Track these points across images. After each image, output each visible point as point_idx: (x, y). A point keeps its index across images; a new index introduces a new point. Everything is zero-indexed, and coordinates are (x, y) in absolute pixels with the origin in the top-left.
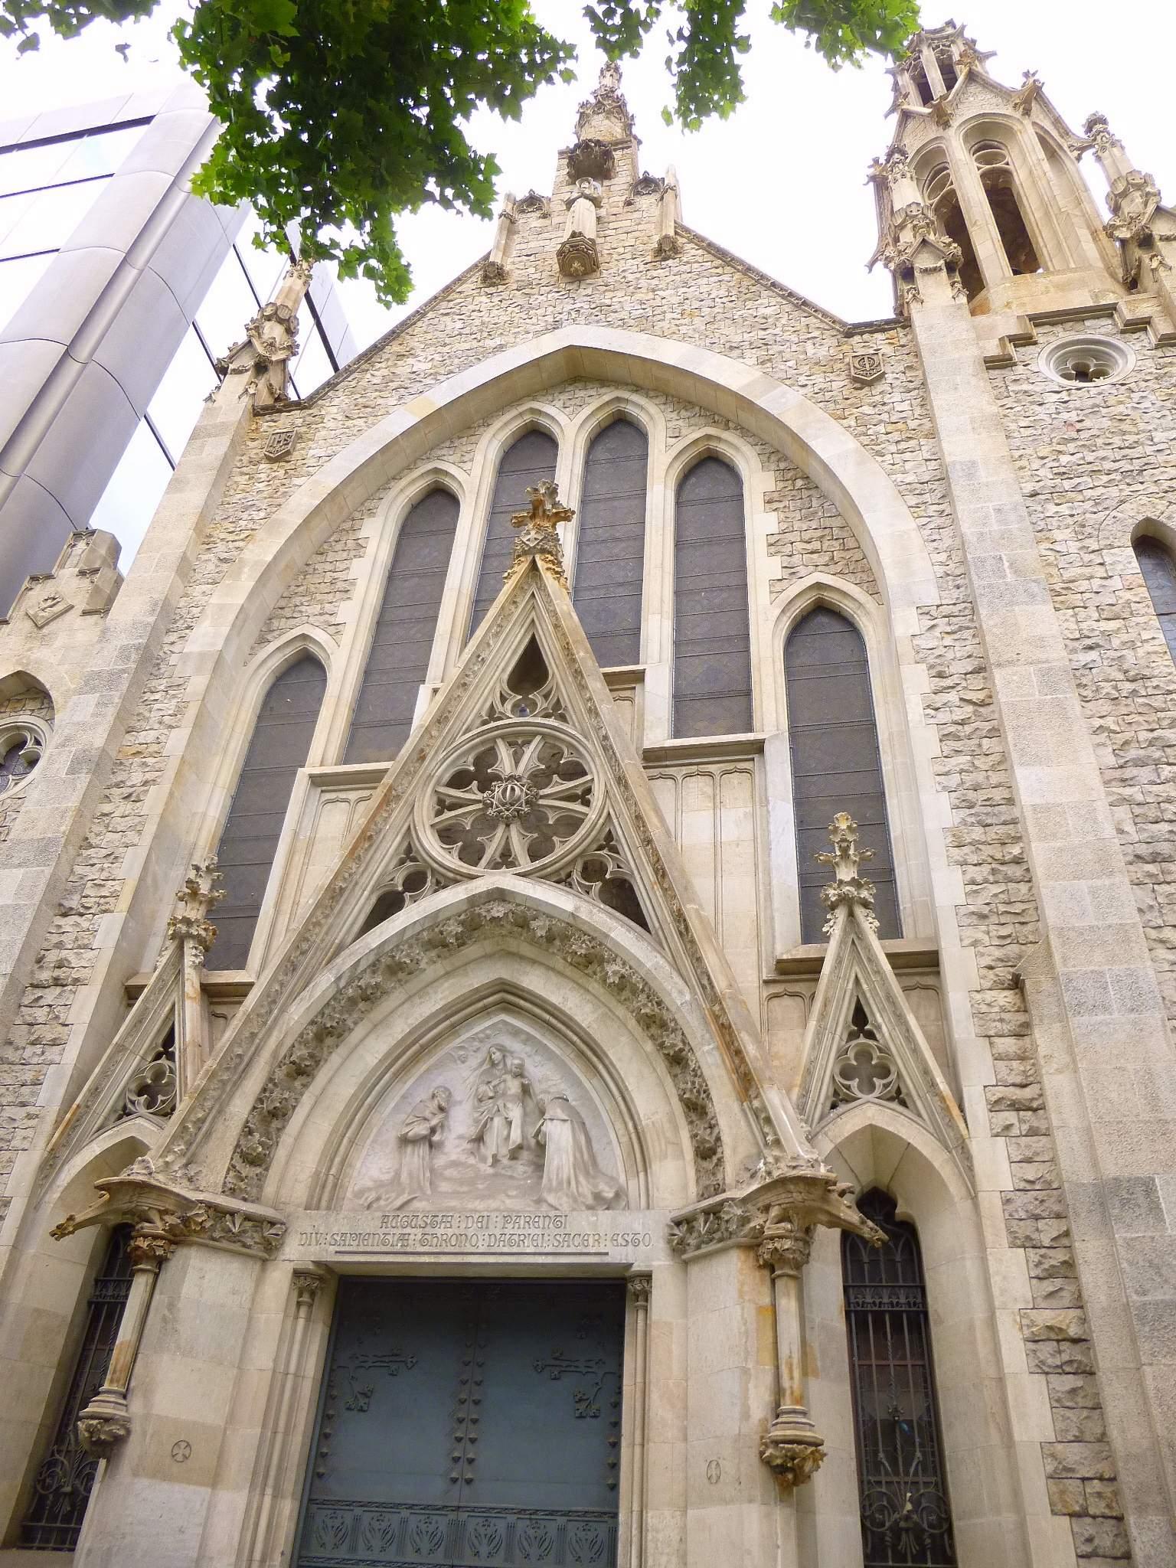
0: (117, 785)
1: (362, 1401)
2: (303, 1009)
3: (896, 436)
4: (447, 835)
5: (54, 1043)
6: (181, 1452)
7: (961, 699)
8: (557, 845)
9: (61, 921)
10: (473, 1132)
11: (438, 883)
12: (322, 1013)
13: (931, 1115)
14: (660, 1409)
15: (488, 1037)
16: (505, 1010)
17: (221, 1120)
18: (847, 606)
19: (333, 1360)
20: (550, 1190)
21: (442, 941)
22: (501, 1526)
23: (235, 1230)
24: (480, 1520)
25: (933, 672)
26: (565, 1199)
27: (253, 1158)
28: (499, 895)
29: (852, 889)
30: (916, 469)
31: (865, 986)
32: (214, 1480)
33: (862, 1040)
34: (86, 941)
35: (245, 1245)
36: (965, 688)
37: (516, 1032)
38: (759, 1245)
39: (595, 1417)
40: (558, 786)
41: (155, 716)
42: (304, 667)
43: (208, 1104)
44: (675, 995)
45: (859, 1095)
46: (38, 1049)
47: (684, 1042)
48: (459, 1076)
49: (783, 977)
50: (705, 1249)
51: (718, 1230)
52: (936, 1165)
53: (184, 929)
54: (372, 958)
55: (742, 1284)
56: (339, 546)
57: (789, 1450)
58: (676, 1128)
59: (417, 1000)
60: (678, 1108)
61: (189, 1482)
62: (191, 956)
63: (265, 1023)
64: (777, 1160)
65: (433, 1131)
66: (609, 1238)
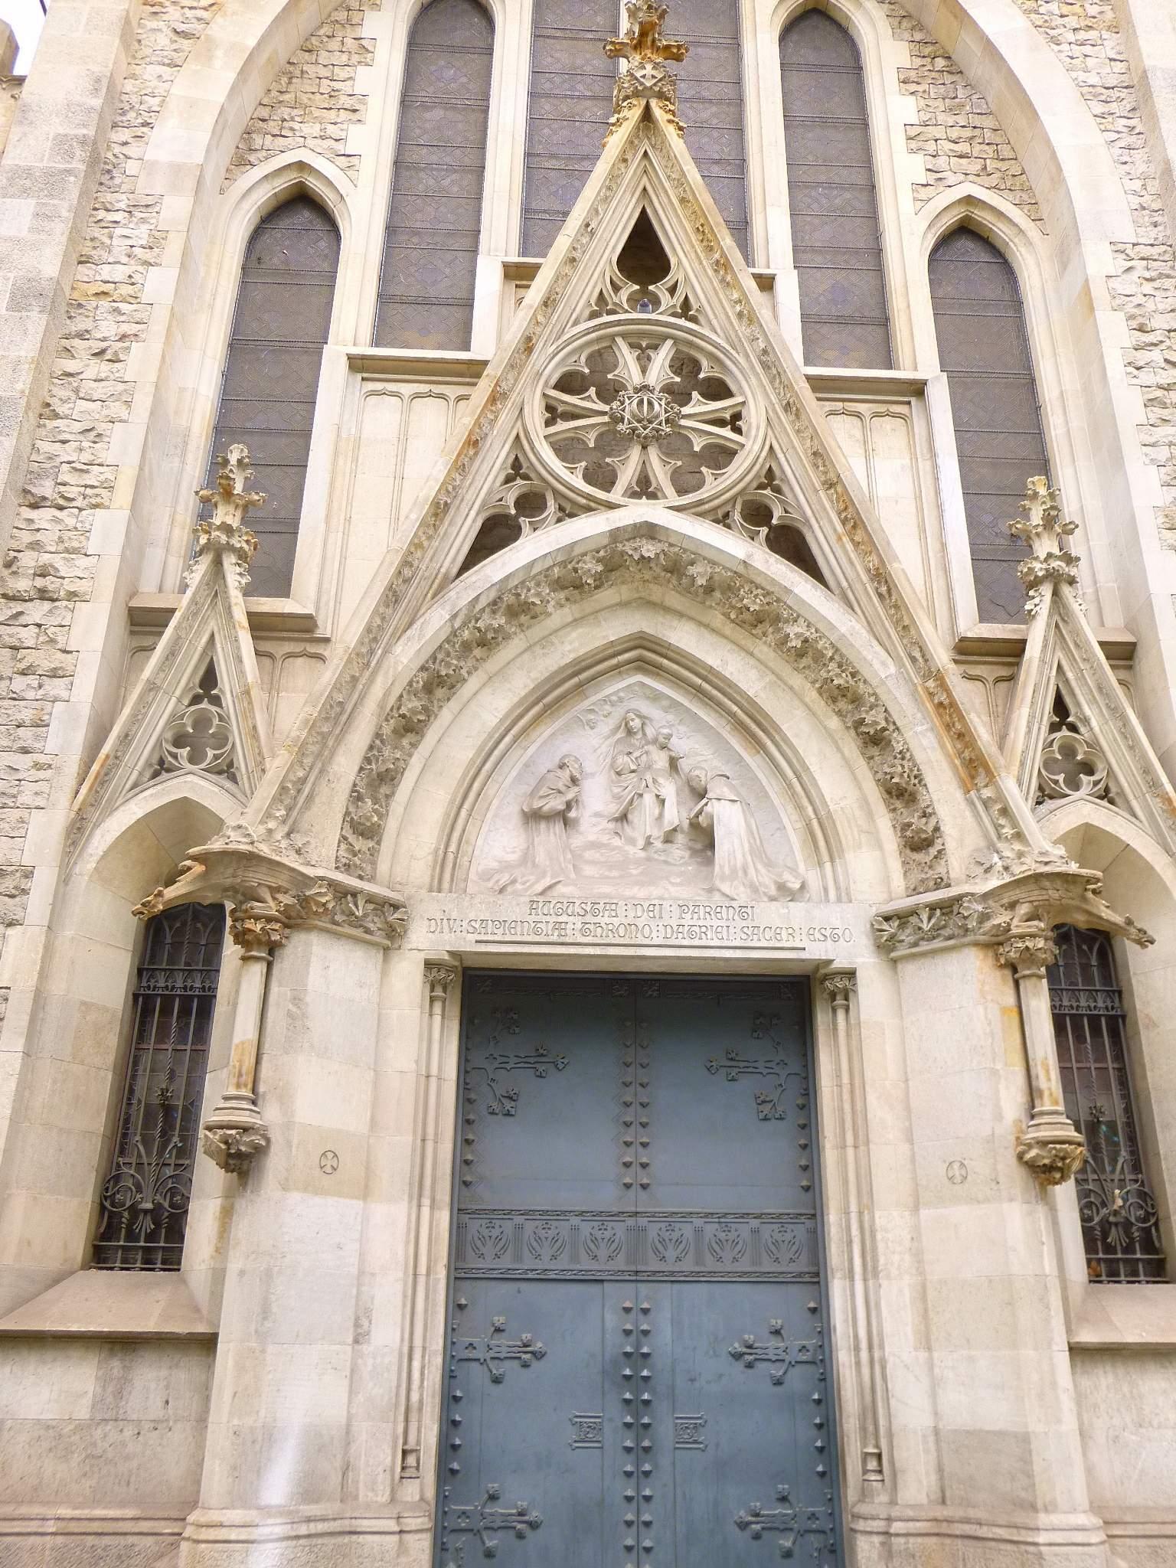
0: (80, 336)
1: (508, 1105)
2: (412, 652)
3: (1072, 22)
4: (565, 449)
5: (54, 674)
6: (329, 1164)
7: (1166, 360)
8: (709, 479)
9: (33, 514)
10: (615, 809)
11: (561, 509)
12: (434, 658)
13: (1151, 816)
14: (881, 1114)
15: (621, 700)
16: (639, 670)
17: (324, 783)
18: (1001, 231)
19: (467, 1060)
20: (723, 878)
21: (569, 580)
22: (688, 1231)
23: (359, 913)
24: (663, 1225)
25: (1134, 324)
26: (742, 889)
27: (364, 830)
28: (649, 531)
29: (1063, 565)
30: (1101, 71)
31: (1070, 675)
32: (365, 1191)
33: (1065, 732)
34: (75, 544)
35: (367, 931)
36: (1169, 348)
37: (656, 697)
38: (1001, 944)
39: (781, 1119)
40: (698, 405)
41: (119, 246)
42: (302, 206)
43: (308, 761)
44: (877, 665)
45: (1069, 792)
46: (33, 680)
47: (886, 720)
48: (587, 743)
49: (963, 658)
50: (925, 946)
51: (944, 927)
52: (1158, 868)
53: (224, 538)
54: (493, 595)
55: (983, 984)
56: (334, 45)
57: (1061, 1150)
58: (870, 815)
59: (538, 650)
60: (874, 794)
61: (340, 1195)
62: (234, 575)
63: (368, 665)
64: (1020, 855)
65: (569, 805)
66: (804, 931)
